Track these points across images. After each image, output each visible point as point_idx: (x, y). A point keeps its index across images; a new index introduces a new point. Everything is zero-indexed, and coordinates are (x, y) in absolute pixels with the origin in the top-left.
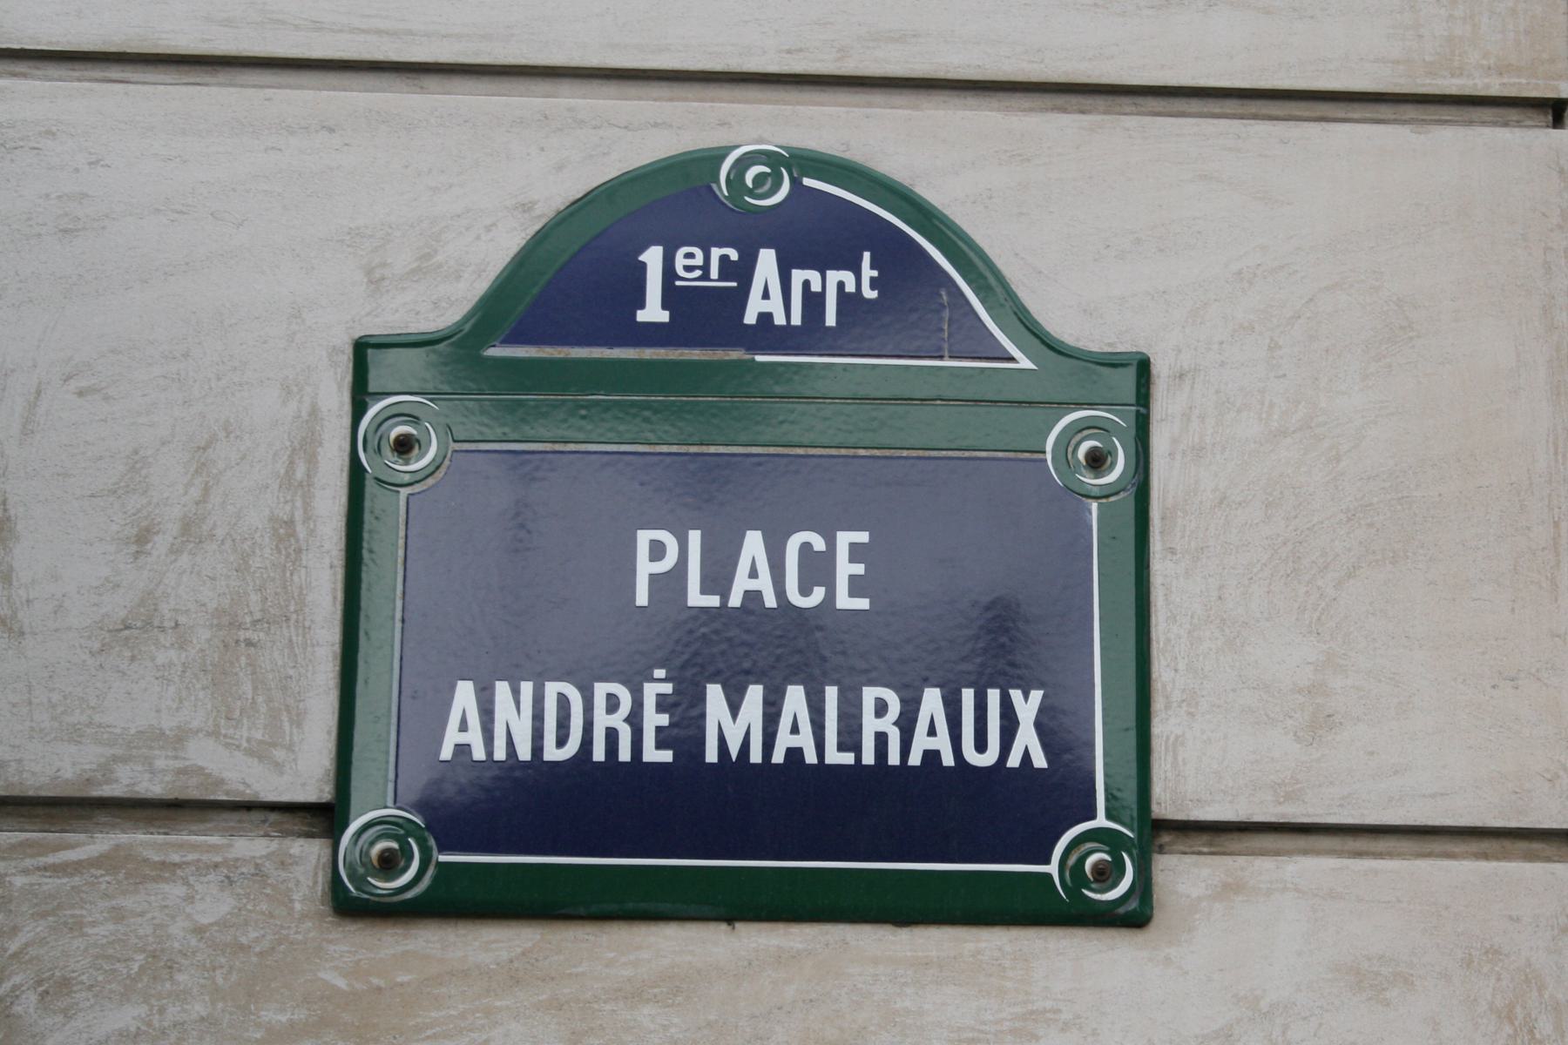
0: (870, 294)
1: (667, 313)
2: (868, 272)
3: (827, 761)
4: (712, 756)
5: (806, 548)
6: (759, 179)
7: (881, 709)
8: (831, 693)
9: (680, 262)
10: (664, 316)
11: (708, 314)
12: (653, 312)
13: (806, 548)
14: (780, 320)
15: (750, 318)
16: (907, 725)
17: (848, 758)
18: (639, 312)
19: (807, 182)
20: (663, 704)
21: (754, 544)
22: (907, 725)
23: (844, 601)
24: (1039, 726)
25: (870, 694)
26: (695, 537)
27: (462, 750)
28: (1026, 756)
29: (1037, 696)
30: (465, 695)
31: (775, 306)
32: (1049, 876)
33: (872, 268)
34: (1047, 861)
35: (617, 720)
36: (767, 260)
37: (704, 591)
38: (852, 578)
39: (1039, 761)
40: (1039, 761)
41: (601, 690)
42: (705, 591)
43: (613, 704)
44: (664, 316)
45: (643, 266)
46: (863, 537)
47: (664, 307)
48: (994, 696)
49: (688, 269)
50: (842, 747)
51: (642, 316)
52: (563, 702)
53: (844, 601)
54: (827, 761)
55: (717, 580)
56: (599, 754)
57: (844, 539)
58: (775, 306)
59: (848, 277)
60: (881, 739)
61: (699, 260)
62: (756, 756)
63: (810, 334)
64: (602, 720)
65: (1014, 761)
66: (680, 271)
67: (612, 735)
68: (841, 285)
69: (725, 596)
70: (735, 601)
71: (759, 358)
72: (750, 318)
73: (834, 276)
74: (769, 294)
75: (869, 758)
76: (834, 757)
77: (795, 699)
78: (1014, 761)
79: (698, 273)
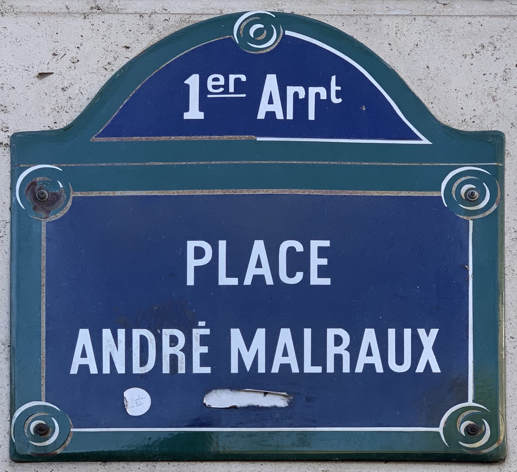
0: (335, 100)
1: (203, 113)
2: (334, 88)
3: (305, 371)
4: (234, 369)
5: (291, 250)
6: (258, 32)
7: (338, 341)
8: (308, 333)
9: (210, 83)
10: (201, 116)
11: (233, 115)
12: (194, 113)
13: (291, 250)
14: (280, 116)
15: (261, 116)
16: (354, 349)
17: (318, 370)
18: (185, 114)
19: (287, 33)
20: (204, 340)
21: (259, 248)
22: (354, 349)
23: (315, 280)
24: (436, 348)
25: (331, 333)
26: (222, 245)
27: (84, 368)
28: (428, 365)
29: (434, 332)
30: (84, 336)
31: (277, 108)
32: (438, 433)
33: (337, 85)
34: (438, 426)
35: (177, 350)
36: (271, 82)
37: (228, 276)
38: (320, 267)
39: (436, 368)
40: (436, 368)
41: (167, 333)
42: (229, 275)
43: (174, 341)
44: (201, 116)
45: (188, 86)
46: (326, 243)
47: (201, 110)
48: (408, 333)
49: (214, 87)
50: (314, 363)
51: (187, 116)
52: (143, 340)
53: (315, 280)
54: (305, 371)
55: (237, 268)
56: (166, 369)
57: (315, 245)
58: (277, 108)
59: (322, 91)
60: (338, 358)
61: (222, 82)
62: (262, 369)
63: (299, 124)
64: (167, 350)
65: (420, 369)
66: (210, 89)
67: (174, 358)
68: (318, 95)
69: (241, 280)
70: (248, 281)
71: (259, 139)
72: (261, 116)
73: (313, 91)
74: (273, 100)
75: (330, 368)
76: (309, 368)
77: (285, 336)
78: (420, 369)
79: (221, 90)
